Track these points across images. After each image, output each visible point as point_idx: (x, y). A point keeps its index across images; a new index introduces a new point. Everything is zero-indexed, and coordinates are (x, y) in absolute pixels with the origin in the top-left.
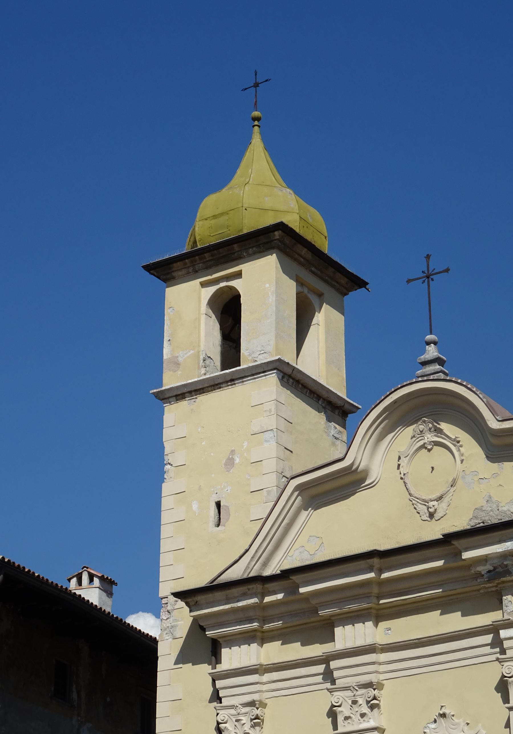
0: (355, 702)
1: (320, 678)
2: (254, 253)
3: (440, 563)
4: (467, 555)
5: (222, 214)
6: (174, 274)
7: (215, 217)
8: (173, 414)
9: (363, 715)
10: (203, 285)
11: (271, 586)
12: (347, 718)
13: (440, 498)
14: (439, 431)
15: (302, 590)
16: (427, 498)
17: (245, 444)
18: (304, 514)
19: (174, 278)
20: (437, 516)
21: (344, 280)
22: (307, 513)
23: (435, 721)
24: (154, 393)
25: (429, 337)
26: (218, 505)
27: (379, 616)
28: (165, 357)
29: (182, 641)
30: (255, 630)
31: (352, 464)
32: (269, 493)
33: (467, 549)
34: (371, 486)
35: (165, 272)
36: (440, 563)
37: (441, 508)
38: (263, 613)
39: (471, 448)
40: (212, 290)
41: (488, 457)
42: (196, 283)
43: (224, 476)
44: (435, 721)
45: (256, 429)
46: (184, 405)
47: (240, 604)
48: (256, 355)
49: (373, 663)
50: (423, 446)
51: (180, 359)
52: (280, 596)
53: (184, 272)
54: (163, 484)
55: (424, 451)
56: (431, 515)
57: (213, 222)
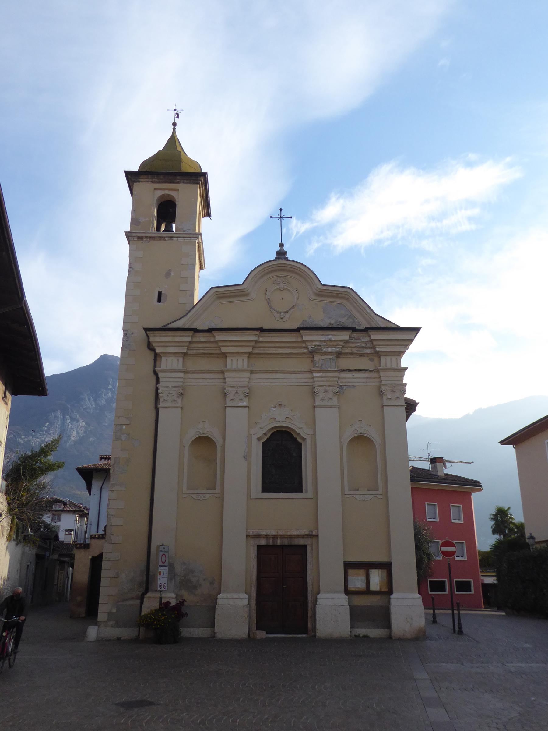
0: (237, 393)
2: (187, 183)
13: (287, 312)
26: (160, 294)
40: (159, 193)
50: (279, 289)
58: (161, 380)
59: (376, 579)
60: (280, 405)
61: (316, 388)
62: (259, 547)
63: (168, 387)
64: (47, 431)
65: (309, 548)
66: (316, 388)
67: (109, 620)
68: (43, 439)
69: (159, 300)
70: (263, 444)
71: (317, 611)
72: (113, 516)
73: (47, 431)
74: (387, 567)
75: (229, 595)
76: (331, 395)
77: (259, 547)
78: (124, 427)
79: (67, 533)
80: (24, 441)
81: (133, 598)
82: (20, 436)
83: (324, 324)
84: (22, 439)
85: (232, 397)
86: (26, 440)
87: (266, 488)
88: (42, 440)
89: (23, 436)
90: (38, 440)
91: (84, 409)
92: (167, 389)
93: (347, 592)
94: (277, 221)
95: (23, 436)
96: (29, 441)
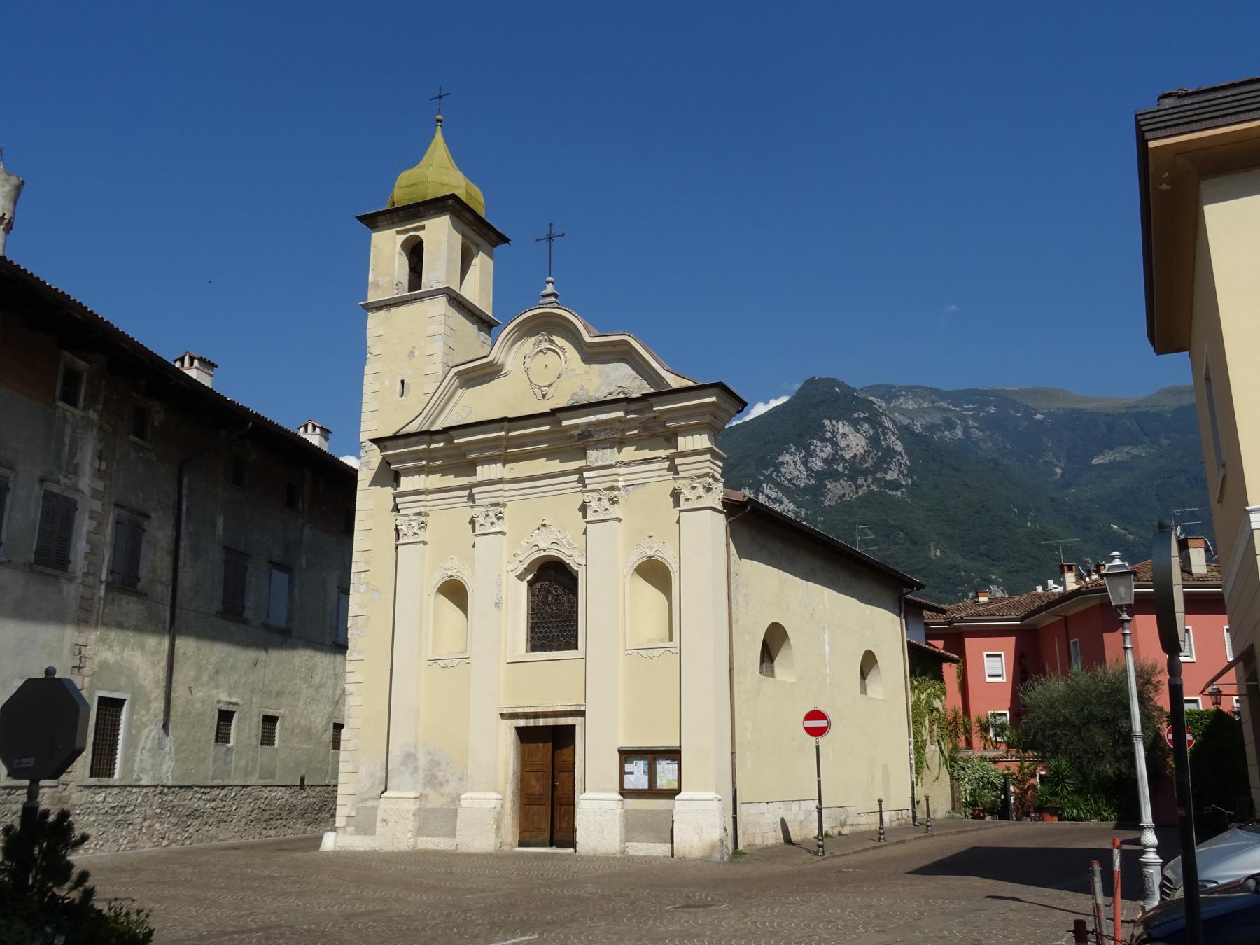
4: (565, 423)
8: (374, 319)
10: (399, 233)
13: (550, 386)
14: (552, 341)
18: (460, 391)
21: (494, 237)
25: (549, 279)
27: (506, 460)
34: (505, 375)
35: (373, 221)
37: (550, 392)
38: (430, 455)
40: (404, 236)
43: (406, 364)
46: (382, 313)
52: (441, 445)
56: (544, 396)
59: (666, 773)
60: (544, 525)
62: (519, 730)
65: (578, 729)
67: (348, 825)
75: (475, 795)
77: (519, 730)
91: (790, 481)
93: (625, 793)
94: (545, 244)
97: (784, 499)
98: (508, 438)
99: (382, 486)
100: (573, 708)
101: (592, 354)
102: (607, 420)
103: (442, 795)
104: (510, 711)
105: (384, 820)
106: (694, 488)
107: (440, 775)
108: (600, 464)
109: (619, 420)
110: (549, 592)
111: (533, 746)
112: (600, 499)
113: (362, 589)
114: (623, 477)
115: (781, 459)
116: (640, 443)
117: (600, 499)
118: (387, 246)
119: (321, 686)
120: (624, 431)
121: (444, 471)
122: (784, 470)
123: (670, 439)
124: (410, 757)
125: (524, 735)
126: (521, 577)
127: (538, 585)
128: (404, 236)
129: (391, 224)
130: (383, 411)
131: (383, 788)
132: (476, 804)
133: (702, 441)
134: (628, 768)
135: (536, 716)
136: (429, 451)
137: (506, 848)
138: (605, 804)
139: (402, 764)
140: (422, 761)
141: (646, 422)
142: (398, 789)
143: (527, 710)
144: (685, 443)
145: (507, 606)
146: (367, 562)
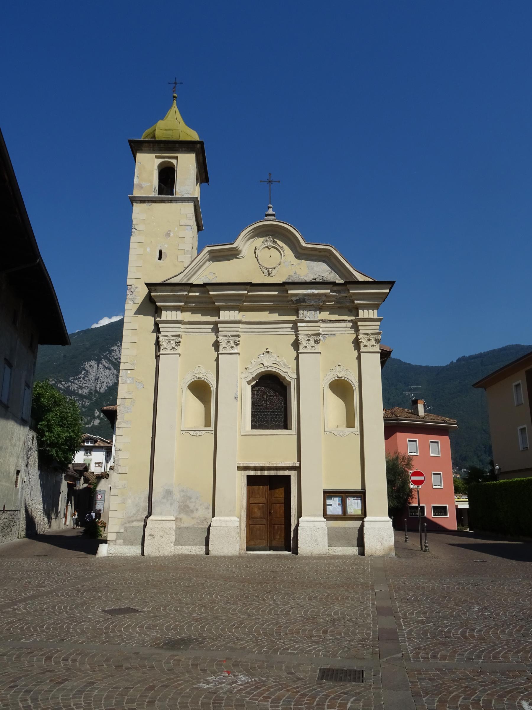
1: (210, 330)
2: (185, 151)
3: (276, 293)
4: (290, 292)
5: (169, 130)
6: (143, 148)
7: (166, 130)
8: (137, 208)
9: (232, 347)
10: (156, 157)
11: (193, 289)
12: (224, 348)
13: (274, 268)
14: (275, 242)
15: (211, 293)
16: (268, 267)
17: (176, 229)
18: (208, 263)
19: (142, 150)
20: (271, 275)
21: (204, 177)
22: (209, 263)
23: (263, 354)
24: (130, 197)
25: (270, 205)
26: (160, 252)
27: (241, 309)
28: (135, 183)
29: (138, 305)
30: (181, 306)
31: (237, 247)
32: (187, 251)
33: (290, 290)
34: (241, 258)
35: (137, 146)
36: (276, 293)
37: (274, 272)
38: (187, 299)
39: (288, 251)
40: (161, 160)
41: (295, 257)
42: (154, 155)
43: (162, 239)
44: (263, 354)
45: (183, 224)
46: (144, 205)
47: (178, 294)
48: (183, 193)
49: (239, 327)
50: (267, 247)
51: (143, 185)
52: (198, 294)
53: (148, 148)
54: (131, 237)
55: (267, 249)
56: (269, 274)
57: (164, 131)
58: (161, 330)
61: (300, 336)
62: (249, 477)
63: (168, 336)
64: (84, 379)
66: (300, 336)
68: (81, 385)
69: (160, 258)
70: (253, 387)
71: (299, 531)
72: (120, 450)
73: (84, 379)
74: (361, 495)
75: (222, 518)
76: (373, 342)
77: (249, 477)
78: (129, 372)
79: (97, 465)
80: (64, 386)
81: (138, 521)
82: (60, 382)
83: (309, 279)
84: (62, 384)
85: (305, 345)
86: (66, 386)
87: (254, 426)
88: (80, 386)
89: (63, 383)
90: (76, 386)
91: (116, 359)
92: (167, 338)
93: (325, 516)
95: (63, 383)
96: (69, 386)
97: (112, 368)
98: (247, 296)
99: (145, 315)
100: (291, 465)
101: (301, 254)
102: (318, 294)
103: (193, 518)
104: (245, 465)
105: (151, 535)
106: (369, 340)
107: (192, 506)
108: (307, 319)
109: (325, 295)
110: (264, 393)
111: (256, 488)
112: (308, 340)
113: (129, 381)
114: (323, 328)
115: (113, 348)
116: (332, 310)
117: (308, 340)
118: (147, 165)
119: (15, 445)
120: (324, 302)
121: (193, 311)
122: (113, 354)
123: (354, 310)
124: (169, 493)
125: (251, 481)
126: (249, 383)
127: (257, 389)
128: (161, 160)
129: (152, 151)
130: (142, 270)
131: (146, 514)
132: (224, 524)
133: (373, 314)
134: (328, 502)
135: (262, 469)
136: (187, 297)
137: (242, 552)
138: (317, 524)
139: (164, 498)
140: (177, 496)
141: (344, 299)
142: (161, 514)
143: (257, 465)
144: (363, 314)
145: (237, 402)
146: (132, 364)
